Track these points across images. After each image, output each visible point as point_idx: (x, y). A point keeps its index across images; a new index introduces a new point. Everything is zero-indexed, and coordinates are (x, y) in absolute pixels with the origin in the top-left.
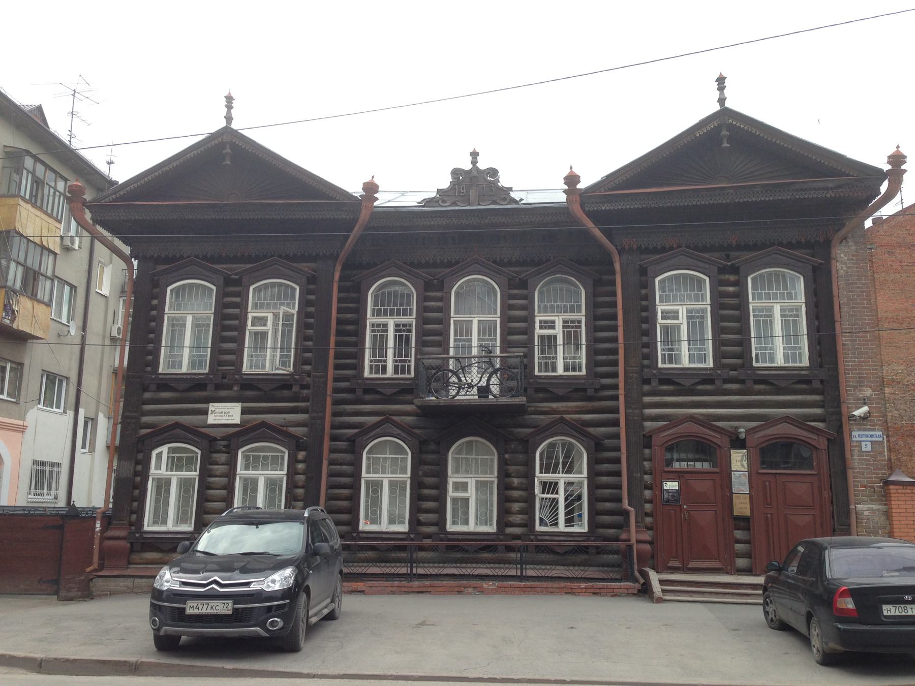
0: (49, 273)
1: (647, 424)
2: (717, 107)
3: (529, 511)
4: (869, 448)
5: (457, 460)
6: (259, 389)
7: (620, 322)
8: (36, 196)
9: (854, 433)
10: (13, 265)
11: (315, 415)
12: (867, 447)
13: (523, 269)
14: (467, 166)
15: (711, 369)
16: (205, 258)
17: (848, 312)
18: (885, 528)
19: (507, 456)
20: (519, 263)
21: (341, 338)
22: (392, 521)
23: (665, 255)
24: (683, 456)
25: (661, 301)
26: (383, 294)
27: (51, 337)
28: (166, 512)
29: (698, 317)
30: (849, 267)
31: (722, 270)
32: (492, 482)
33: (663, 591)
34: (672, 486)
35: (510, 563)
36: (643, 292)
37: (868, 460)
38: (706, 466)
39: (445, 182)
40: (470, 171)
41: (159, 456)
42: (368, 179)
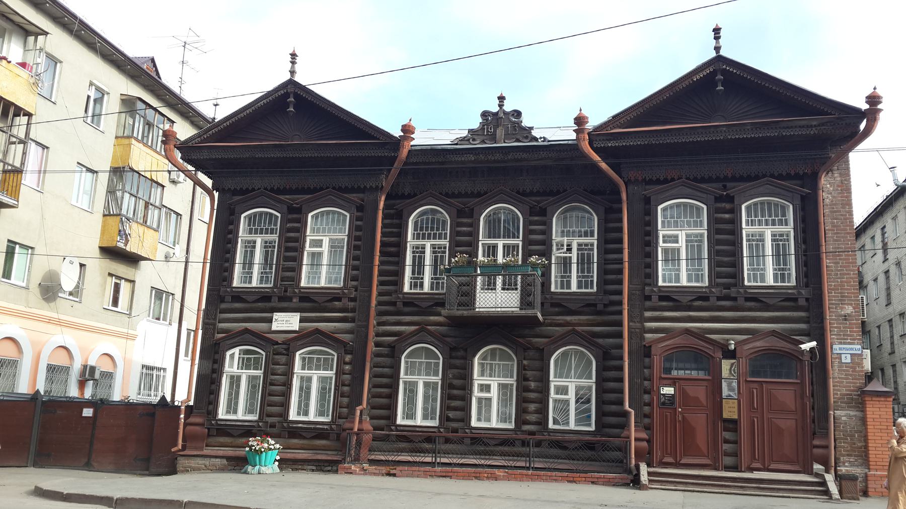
0: (157, 204)
1: (648, 336)
2: (713, 54)
3: (544, 411)
4: (849, 360)
5: (482, 365)
6: (314, 301)
7: (626, 245)
8: (148, 137)
9: (834, 347)
10: (127, 196)
11: (360, 323)
12: (846, 359)
13: (544, 198)
14: (495, 109)
15: (706, 287)
16: (272, 190)
17: (832, 237)
18: (861, 432)
19: (525, 362)
20: (538, 194)
21: (385, 259)
22: (425, 417)
23: (667, 186)
24: (681, 365)
25: (663, 226)
26: (422, 221)
27: (160, 256)
28: (236, 404)
29: (696, 241)
30: (834, 197)
31: (719, 199)
32: (512, 385)
33: (650, 481)
34: (668, 390)
35: (522, 456)
36: (647, 218)
37: (848, 371)
38: (701, 375)
39: (475, 122)
40: (497, 113)
41: (232, 356)
42: (405, 122)
